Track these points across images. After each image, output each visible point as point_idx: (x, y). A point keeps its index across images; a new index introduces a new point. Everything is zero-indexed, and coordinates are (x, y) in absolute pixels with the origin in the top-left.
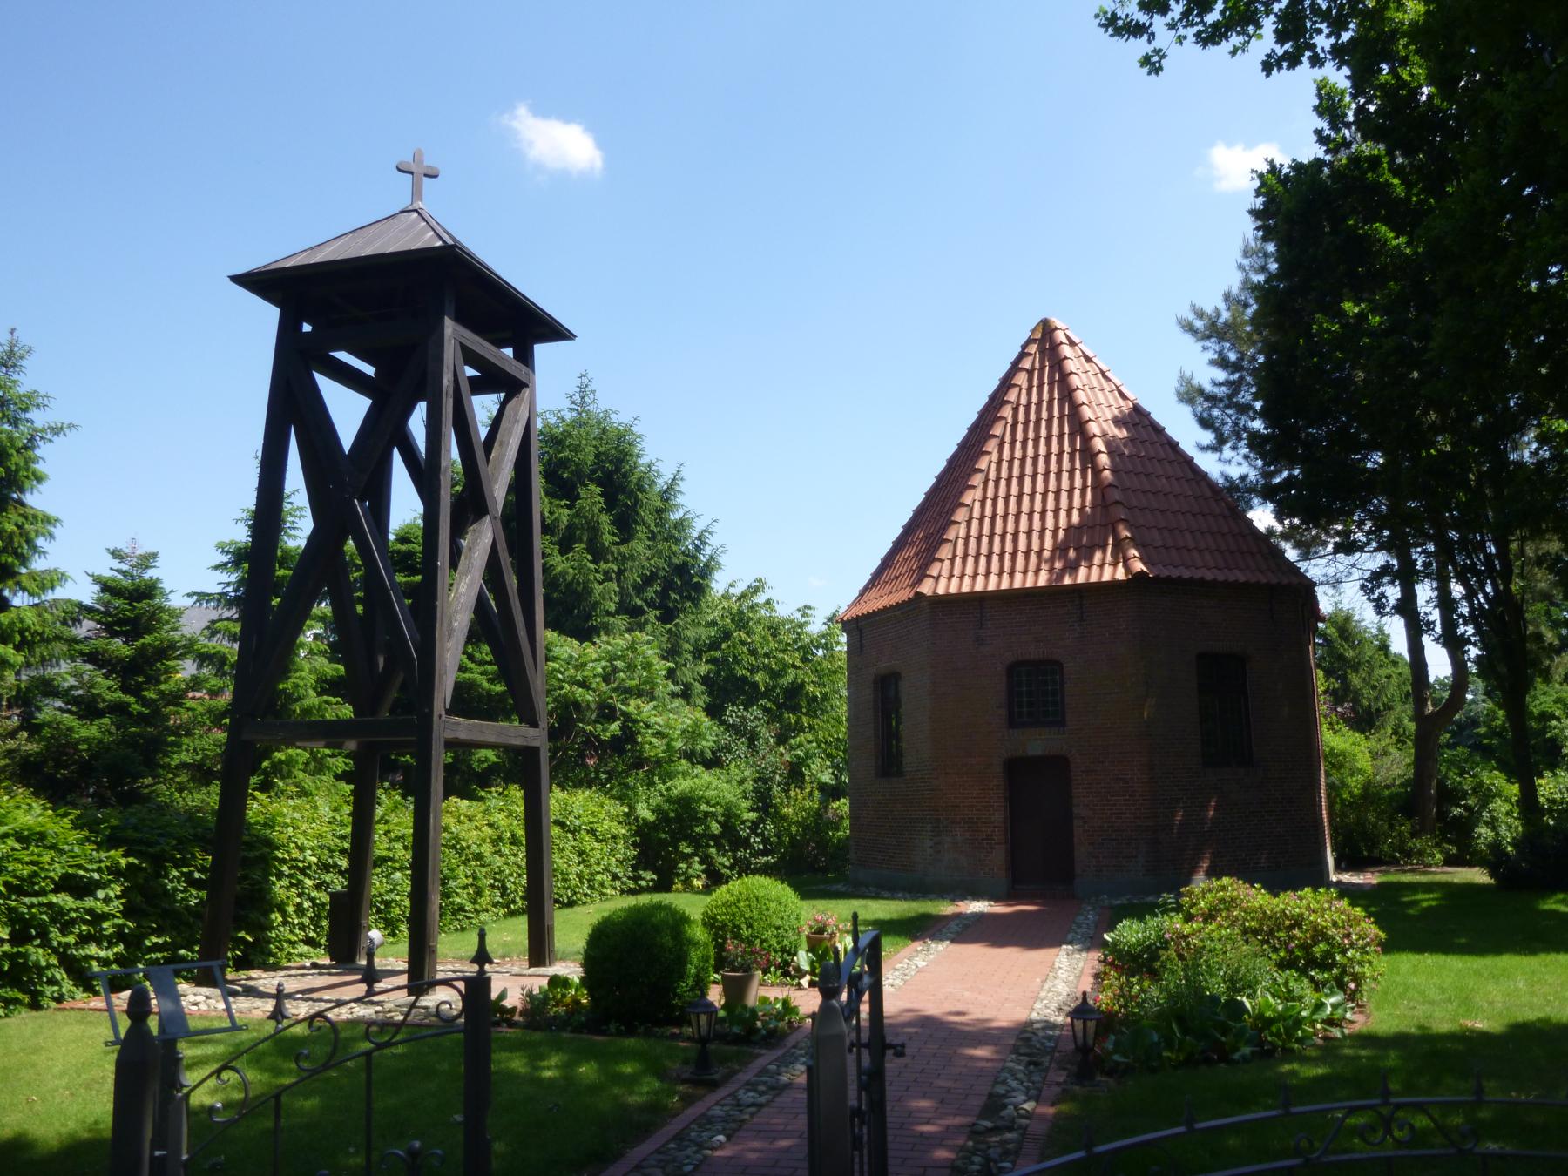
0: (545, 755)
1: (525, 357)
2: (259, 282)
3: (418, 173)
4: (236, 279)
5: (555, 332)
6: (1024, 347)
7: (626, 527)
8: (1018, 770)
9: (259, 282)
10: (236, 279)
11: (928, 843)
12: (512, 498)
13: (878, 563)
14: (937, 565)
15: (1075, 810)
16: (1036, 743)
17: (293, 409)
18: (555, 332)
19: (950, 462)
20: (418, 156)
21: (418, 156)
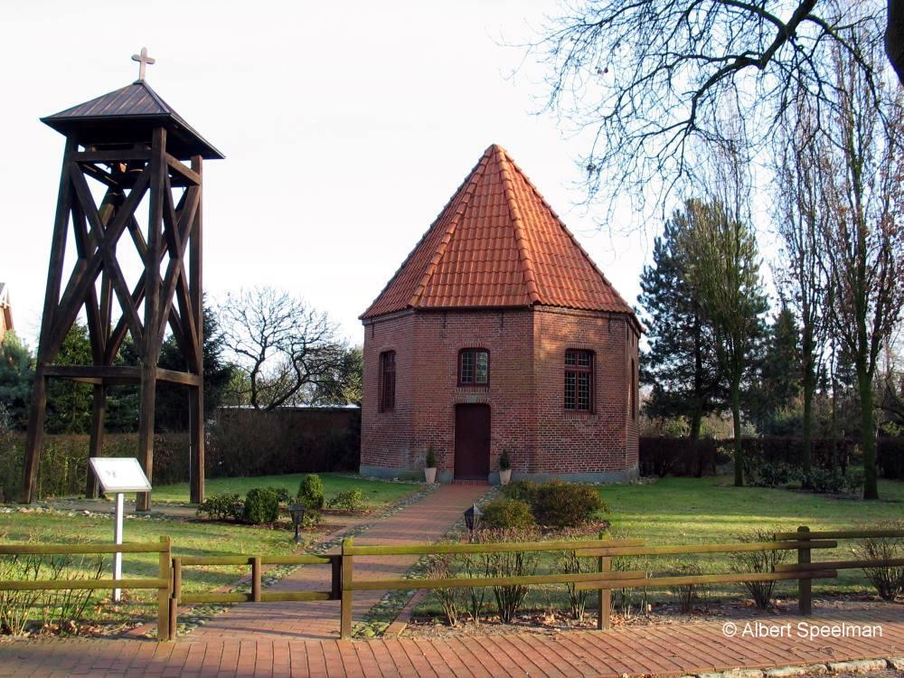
0: (201, 389)
1: (197, 168)
2: (56, 122)
3: (142, 59)
4: (43, 120)
5: (212, 154)
6: (481, 160)
7: (766, 474)
8: (460, 408)
9: (56, 122)
10: (43, 120)
11: (407, 451)
12: (114, 264)
13: (385, 285)
14: (420, 290)
15: (492, 435)
16: (472, 397)
17: (72, 198)
18: (212, 154)
19: (432, 227)
20: (144, 51)
21: (144, 51)
